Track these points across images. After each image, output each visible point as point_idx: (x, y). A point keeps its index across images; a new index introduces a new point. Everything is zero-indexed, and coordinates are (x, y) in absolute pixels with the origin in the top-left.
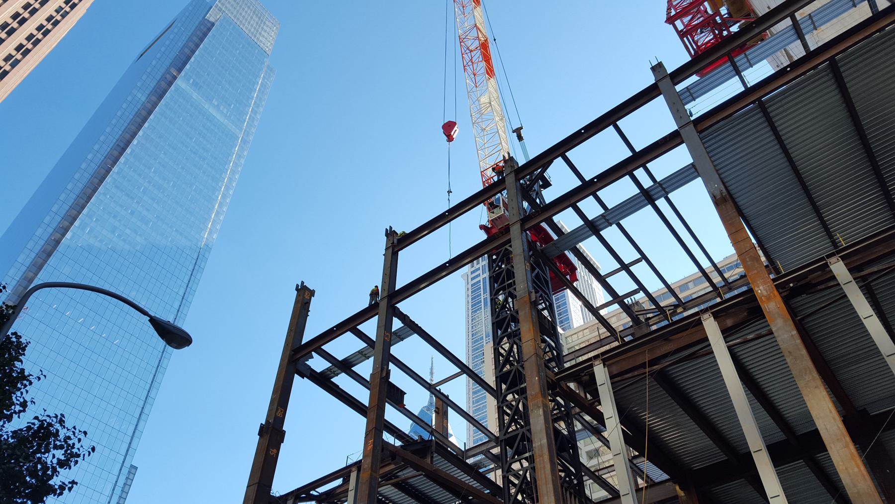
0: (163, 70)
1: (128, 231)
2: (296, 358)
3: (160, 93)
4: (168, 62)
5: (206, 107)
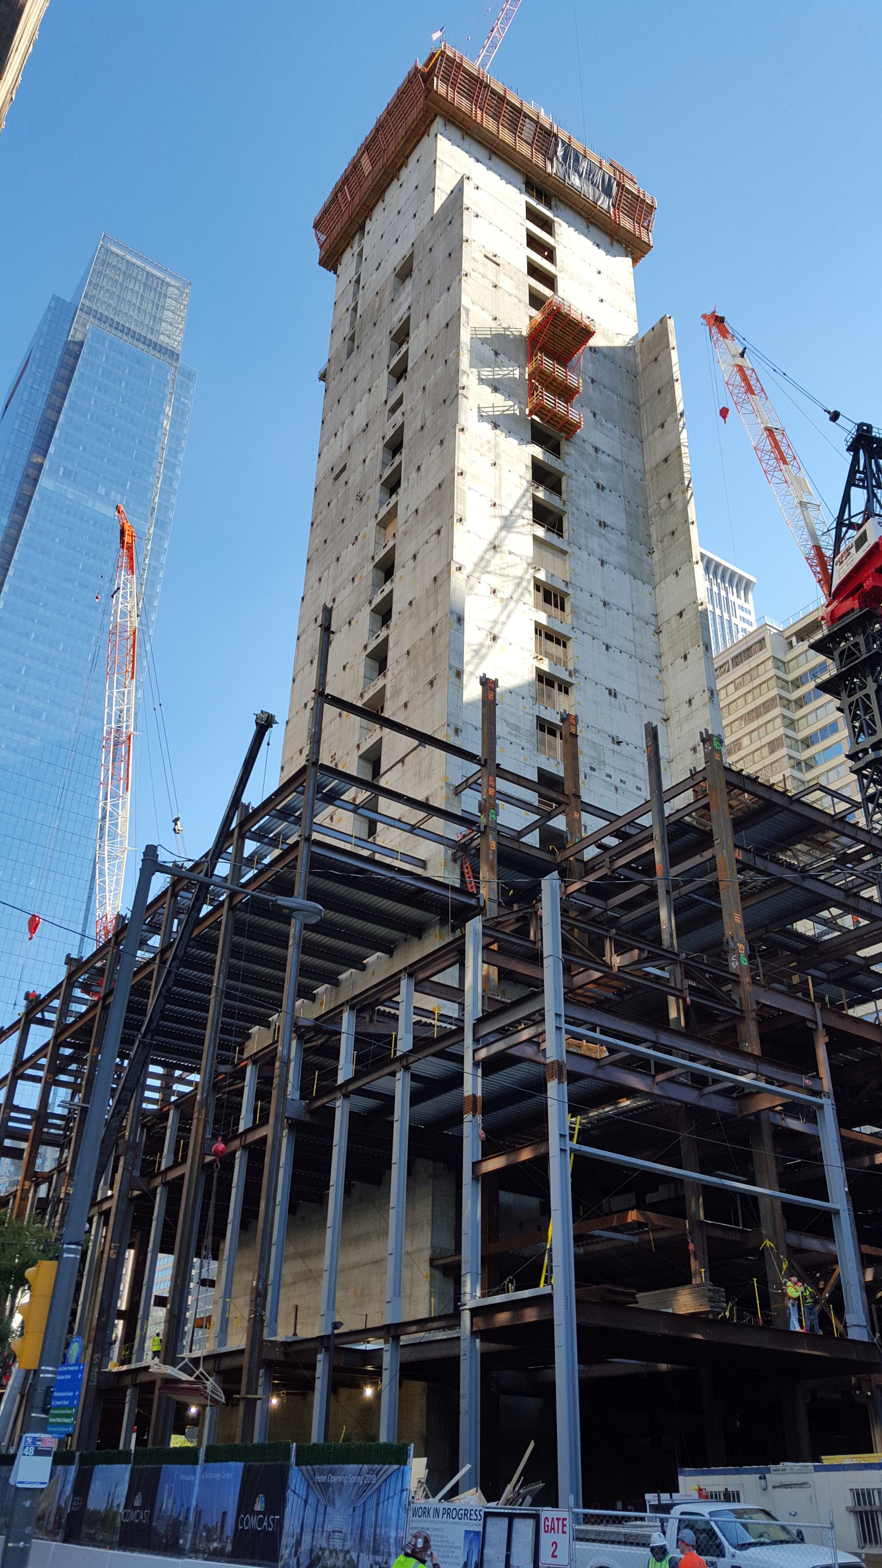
0: (23, 461)
1: (17, 737)
2: (765, 472)
3: (22, 506)
4: (27, 448)
5: (90, 505)
